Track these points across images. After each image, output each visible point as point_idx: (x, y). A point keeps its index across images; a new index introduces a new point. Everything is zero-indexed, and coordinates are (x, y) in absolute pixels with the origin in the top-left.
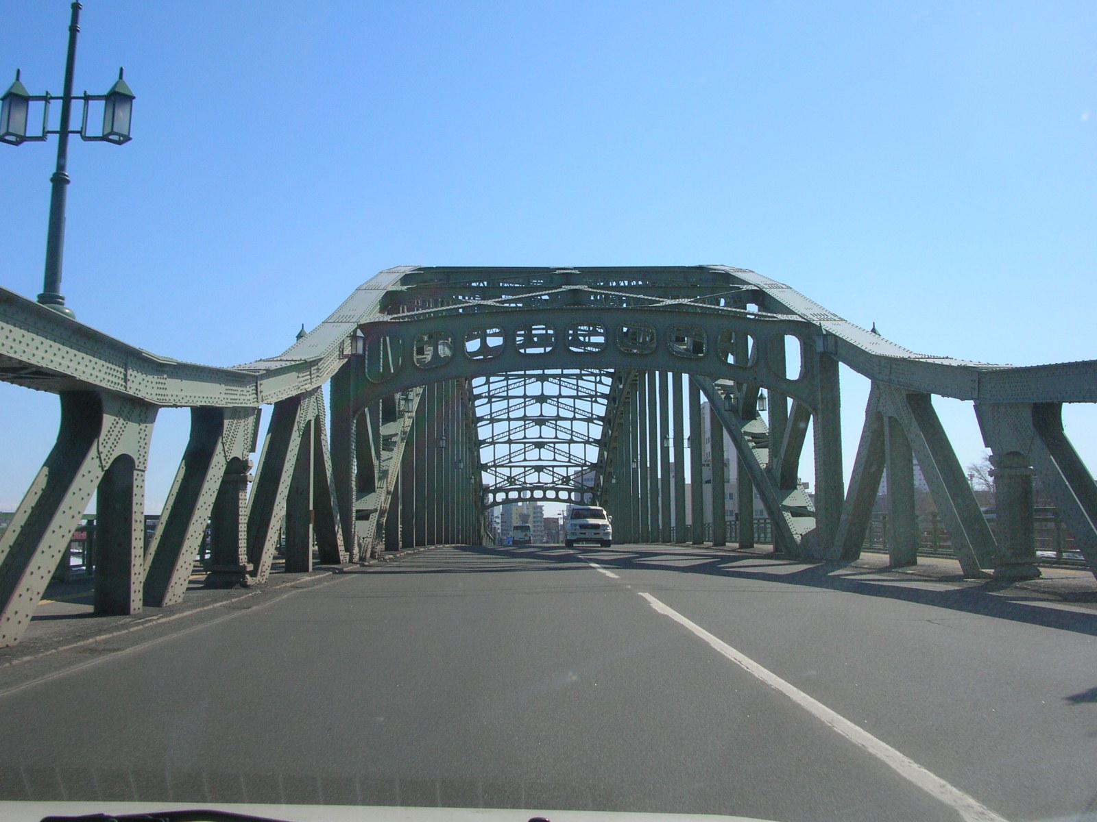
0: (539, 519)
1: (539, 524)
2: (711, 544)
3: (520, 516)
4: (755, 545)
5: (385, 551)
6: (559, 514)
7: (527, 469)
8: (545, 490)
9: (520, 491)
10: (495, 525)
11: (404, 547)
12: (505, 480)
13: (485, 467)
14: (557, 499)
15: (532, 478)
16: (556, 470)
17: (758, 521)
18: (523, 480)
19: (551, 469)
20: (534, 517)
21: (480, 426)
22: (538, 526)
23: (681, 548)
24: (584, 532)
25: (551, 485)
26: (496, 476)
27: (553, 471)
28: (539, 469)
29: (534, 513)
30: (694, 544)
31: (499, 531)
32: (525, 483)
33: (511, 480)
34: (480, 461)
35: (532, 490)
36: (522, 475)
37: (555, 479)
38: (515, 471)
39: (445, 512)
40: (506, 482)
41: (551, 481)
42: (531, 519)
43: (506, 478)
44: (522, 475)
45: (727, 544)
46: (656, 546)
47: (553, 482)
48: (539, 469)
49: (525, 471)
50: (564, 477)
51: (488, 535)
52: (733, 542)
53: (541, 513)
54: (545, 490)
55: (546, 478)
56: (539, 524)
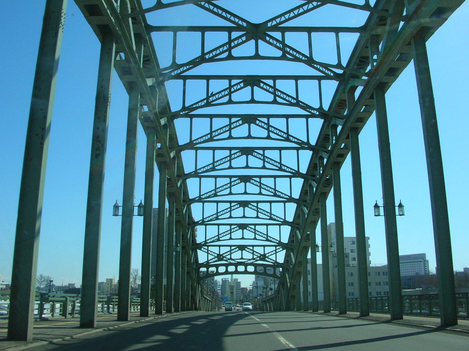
0: (239, 288)
1: (239, 290)
2: (323, 311)
3: (230, 286)
4: (348, 312)
5: (155, 314)
6: (250, 285)
7: (233, 248)
8: (246, 265)
9: (227, 266)
10: (218, 291)
11: (181, 310)
12: (216, 257)
13: (200, 246)
14: (246, 272)
15: (237, 255)
16: (255, 249)
17: (376, 298)
18: (229, 257)
19: (251, 248)
20: (237, 287)
21: (78, 311)
22: (238, 291)
23: (307, 314)
24: (62, 306)
25: (251, 261)
26: (208, 253)
27: (253, 250)
28: (242, 248)
29: (237, 285)
30: (304, 311)
31: (220, 293)
32: (231, 259)
33: (220, 257)
34: (304, 181)
35: (236, 265)
36: (228, 253)
37: (255, 257)
38: (224, 250)
39: (172, 277)
40: (216, 259)
41: (251, 258)
42: (235, 288)
43: (216, 255)
44: (228, 253)
45: (319, 311)
46: (292, 313)
47: (253, 259)
48: (242, 248)
49: (231, 250)
50: (261, 255)
51: (205, 298)
52: (355, 311)
53: (240, 285)
54: (246, 265)
55: (247, 255)
56: (239, 290)
